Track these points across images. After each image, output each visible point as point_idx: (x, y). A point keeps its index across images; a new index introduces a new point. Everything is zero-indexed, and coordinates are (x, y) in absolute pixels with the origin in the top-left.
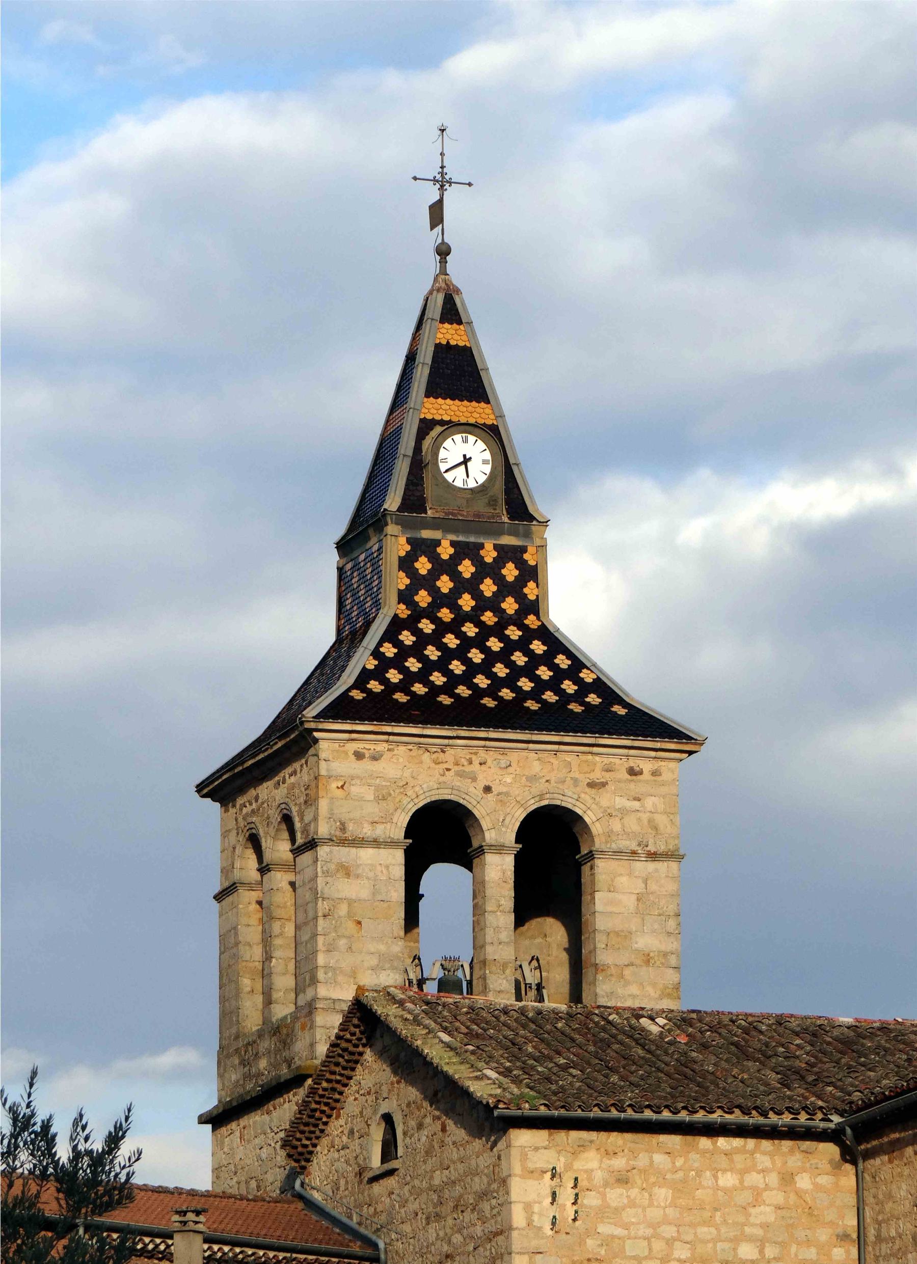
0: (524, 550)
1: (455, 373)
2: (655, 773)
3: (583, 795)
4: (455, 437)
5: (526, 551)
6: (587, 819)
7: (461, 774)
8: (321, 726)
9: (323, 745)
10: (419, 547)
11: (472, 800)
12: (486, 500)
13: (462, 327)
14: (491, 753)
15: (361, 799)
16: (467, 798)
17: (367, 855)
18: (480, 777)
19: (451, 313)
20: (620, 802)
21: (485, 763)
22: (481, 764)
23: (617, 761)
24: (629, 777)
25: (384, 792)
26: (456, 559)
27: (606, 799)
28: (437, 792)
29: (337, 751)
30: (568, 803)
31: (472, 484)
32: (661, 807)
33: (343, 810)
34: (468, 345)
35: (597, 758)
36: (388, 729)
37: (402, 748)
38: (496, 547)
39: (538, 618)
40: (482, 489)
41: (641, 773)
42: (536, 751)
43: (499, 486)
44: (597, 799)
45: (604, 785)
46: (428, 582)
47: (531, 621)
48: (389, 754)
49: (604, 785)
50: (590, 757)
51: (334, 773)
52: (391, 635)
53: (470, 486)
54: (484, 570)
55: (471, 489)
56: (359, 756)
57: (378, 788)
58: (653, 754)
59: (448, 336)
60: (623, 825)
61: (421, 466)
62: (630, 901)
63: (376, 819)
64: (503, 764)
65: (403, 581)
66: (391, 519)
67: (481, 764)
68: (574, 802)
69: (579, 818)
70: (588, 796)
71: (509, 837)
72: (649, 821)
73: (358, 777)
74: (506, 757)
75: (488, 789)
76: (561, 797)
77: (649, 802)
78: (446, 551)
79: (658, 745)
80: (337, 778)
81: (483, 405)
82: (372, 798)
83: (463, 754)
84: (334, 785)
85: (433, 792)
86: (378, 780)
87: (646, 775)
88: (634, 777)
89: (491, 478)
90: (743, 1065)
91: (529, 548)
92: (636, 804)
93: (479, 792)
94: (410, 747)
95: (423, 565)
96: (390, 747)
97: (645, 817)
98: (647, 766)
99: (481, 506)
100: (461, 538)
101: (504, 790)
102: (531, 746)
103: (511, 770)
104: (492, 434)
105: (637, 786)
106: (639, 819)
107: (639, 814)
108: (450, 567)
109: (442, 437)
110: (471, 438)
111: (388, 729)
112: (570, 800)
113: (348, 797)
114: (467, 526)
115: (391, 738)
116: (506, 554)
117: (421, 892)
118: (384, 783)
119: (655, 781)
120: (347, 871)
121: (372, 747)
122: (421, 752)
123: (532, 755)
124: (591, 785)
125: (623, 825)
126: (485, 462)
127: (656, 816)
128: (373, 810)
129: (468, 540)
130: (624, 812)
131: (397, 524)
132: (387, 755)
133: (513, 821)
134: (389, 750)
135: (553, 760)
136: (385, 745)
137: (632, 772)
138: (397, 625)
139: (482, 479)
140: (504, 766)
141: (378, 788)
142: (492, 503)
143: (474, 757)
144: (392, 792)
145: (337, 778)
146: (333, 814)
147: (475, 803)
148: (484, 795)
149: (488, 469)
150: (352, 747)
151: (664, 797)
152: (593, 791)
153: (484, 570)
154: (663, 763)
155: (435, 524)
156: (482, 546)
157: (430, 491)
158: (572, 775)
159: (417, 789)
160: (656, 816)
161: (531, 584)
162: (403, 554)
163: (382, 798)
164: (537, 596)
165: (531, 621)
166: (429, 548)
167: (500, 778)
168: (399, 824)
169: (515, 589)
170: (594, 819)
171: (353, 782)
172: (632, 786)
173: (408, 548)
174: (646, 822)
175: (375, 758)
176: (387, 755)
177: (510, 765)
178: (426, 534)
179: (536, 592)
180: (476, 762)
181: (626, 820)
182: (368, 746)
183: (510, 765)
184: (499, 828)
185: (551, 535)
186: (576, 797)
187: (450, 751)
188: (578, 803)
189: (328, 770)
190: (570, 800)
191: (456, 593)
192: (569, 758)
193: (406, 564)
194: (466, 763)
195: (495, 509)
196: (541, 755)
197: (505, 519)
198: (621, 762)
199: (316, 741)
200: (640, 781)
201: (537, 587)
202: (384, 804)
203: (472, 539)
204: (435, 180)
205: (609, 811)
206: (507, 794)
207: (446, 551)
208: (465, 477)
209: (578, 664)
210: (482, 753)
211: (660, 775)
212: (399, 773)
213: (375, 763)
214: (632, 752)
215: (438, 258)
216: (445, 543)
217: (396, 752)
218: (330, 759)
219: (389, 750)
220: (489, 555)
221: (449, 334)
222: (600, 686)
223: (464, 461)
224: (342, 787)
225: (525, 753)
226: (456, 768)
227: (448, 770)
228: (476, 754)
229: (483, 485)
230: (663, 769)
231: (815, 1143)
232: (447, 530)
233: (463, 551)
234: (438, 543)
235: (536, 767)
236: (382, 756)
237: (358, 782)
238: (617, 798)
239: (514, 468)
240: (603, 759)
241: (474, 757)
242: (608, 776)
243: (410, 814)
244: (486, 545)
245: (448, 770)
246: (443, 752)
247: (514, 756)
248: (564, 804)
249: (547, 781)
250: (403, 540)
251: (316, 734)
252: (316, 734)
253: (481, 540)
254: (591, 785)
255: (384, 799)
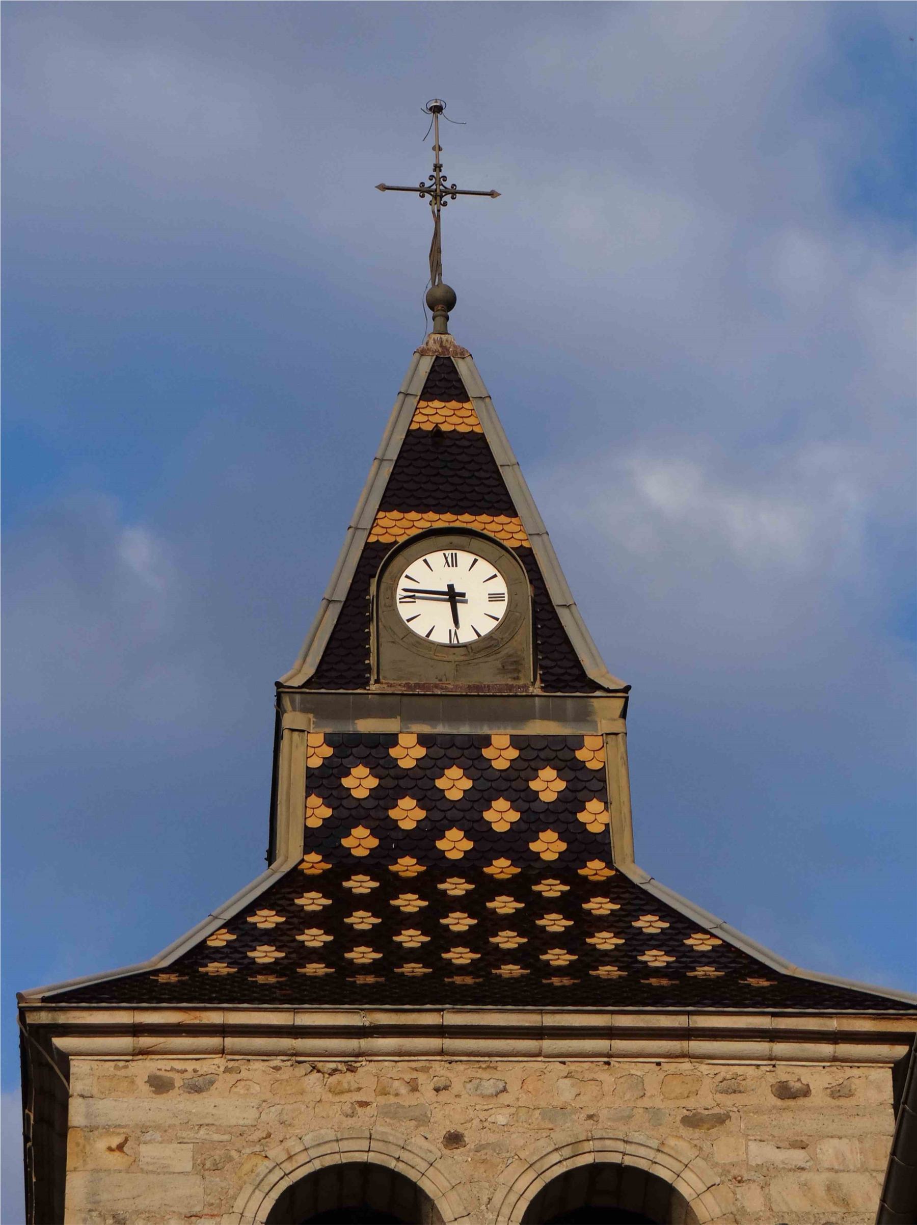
0: (579, 742)
1: (449, 481)
2: (837, 1092)
3: (672, 1142)
4: (429, 557)
5: (581, 746)
6: (683, 1189)
7: (392, 1113)
8: (63, 1018)
9: (78, 1066)
10: (348, 749)
11: (417, 1161)
12: (498, 664)
13: (466, 405)
14: (461, 1067)
15: (165, 1170)
16: (405, 1156)
18: (437, 1115)
19: (444, 382)
20: (762, 1153)
21: (446, 1088)
22: (437, 1090)
23: (751, 1071)
24: (779, 1103)
25: (218, 1154)
26: (431, 767)
27: (726, 1148)
28: (335, 1147)
29: (111, 1078)
30: (639, 1158)
31: (466, 636)
32: (854, 1160)
34: (477, 430)
35: (704, 1068)
36: (215, 1018)
37: (258, 1066)
38: (516, 741)
39: (610, 865)
40: (486, 645)
41: (806, 1092)
42: (562, 1056)
43: (524, 642)
44: (706, 1146)
45: (721, 1120)
46: (374, 814)
47: (594, 869)
48: (231, 1078)
49: (721, 1120)
50: (686, 1066)
51: (102, 1121)
53: (462, 640)
54: (489, 785)
55: (465, 646)
56: (159, 1085)
57: (201, 1147)
58: (826, 1049)
59: (438, 419)
60: (768, 1199)
63: (197, 1209)
64: (489, 1087)
65: (319, 812)
66: (292, 702)
67: (437, 1090)
68: (651, 1154)
69: (669, 1190)
70: (682, 1144)
72: (829, 1189)
73: (157, 1127)
74: (497, 1075)
75: (454, 1140)
76: (621, 1146)
77: (828, 1151)
78: (408, 753)
79: (833, 1025)
80: (108, 1130)
81: (502, 519)
82: (188, 1167)
83: (396, 1072)
84: (101, 1145)
85: (326, 1149)
86: (202, 1131)
87: (818, 1098)
88: (791, 1103)
89: (507, 624)
91: (587, 741)
92: (798, 1156)
93: (436, 1147)
94: (277, 1061)
95: (360, 782)
96: (231, 1064)
97: (819, 1180)
98: (818, 1079)
99: (486, 675)
100: (441, 729)
101: (492, 1138)
102: (548, 1045)
103: (505, 1099)
105: (797, 1120)
106: (805, 1187)
107: (804, 1176)
109: (600, 800)
110: (465, 558)
111: (215, 1018)
112: (642, 1151)
113: (134, 1165)
115: (231, 1042)
116: (534, 753)
118: (216, 1137)
119: (839, 1107)
121: (190, 1066)
122: (301, 1070)
123: (556, 1067)
124: (692, 1121)
125: (768, 1199)
126: (494, 598)
127: (844, 1178)
129: (455, 732)
130: (768, 1173)
131: (304, 710)
132: (223, 1082)
133: (513, 1198)
134: (227, 1070)
135: (605, 1077)
136: (219, 1062)
137: (785, 1092)
139: (487, 627)
140: (492, 1091)
141: (201, 1147)
142: (512, 666)
143: (422, 1078)
144: (234, 1154)
145: (108, 1130)
146: (97, 1202)
147: (423, 1166)
148: (446, 1152)
149: (500, 609)
150: (144, 1068)
151: (861, 1139)
152: (697, 1133)
153: (489, 785)
154: (855, 1072)
155: (388, 705)
156: (486, 741)
157: (384, 656)
158: (646, 1103)
159: (289, 1143)
160: (844, 1178)
161: (594, 806)
162: (315, 762)
163: (209, 1164)
164: (607, 825)
165: (594, 869)
166: (375, 750)
167: (483, 1115)
168: (249, 1215)
169: (563, 815)
170: (701, 1187)
171: (148, 1137)
172: (787, 1119)
173: (328, 751)
174: (821, 1192)
175: (196, 1089)
176: (223, 1082)
177: (504, 1090)
178: (366, 726)
179: (604, 818)
180: (426, 1084)
181: (774, 1190)
182: (179, 1065)
183: (504, 1090)
186: (654, 1144)
187: (366, 1069)
188: (660, 1158)
189: (88, 1115)
190: (642, 1151)
191: (431, 830)
192: (637, 1069)
193: (323, 781)
194: (404, 1090)
195: (518, 678)
196: (573, 1066)
197: (536, 690)
198: (759, 1072)
199: (64, 1059)
200: (803, 1109)
201: (606, 809)
202: (216, 1179)
203: (465, 729)
204: (422, 190)
205: (735, 1172)
206: (497, 1147)
207: (408, 753)
208: (453, 628)
210: (439, 1067)
211: (850, 1095)
212: (251, 1115)
213: (196, 1096)
214: (781, 1048)
215: (430, 313)
216: (407, 740)
217: (244, 1074)
218: (95, 1091)
219: (227, 1070)
220: (501, 754)
221: (442, 415)
224: (120, 1147)
225: (536, 1065)
226: (382, 1100)
227: (364, 1104)
228: (425, 1070)
229: (490, 636)
230: (856, 1084)
232: (410, 717)
234: (392, 740)
235: (566, 1091)
236: (212, 1083)
237: (158, 1136)
238: (753, 1146)
239: (565, 617)
240: (717, 1069)
241: (422, 1078)
242: (728, 1101)
243: (275, 1195)
244: (495, 740)
245: (364, 1104)
246: (352, 1070)
247: (512, 1072)
248: (628, 1161)
249: (590, 1117)
250: (317, 739)
251: (60, 1042)
252: (60, 1042)
253: (485, 730)
254: (692, 1121)
255: (216, 1168)
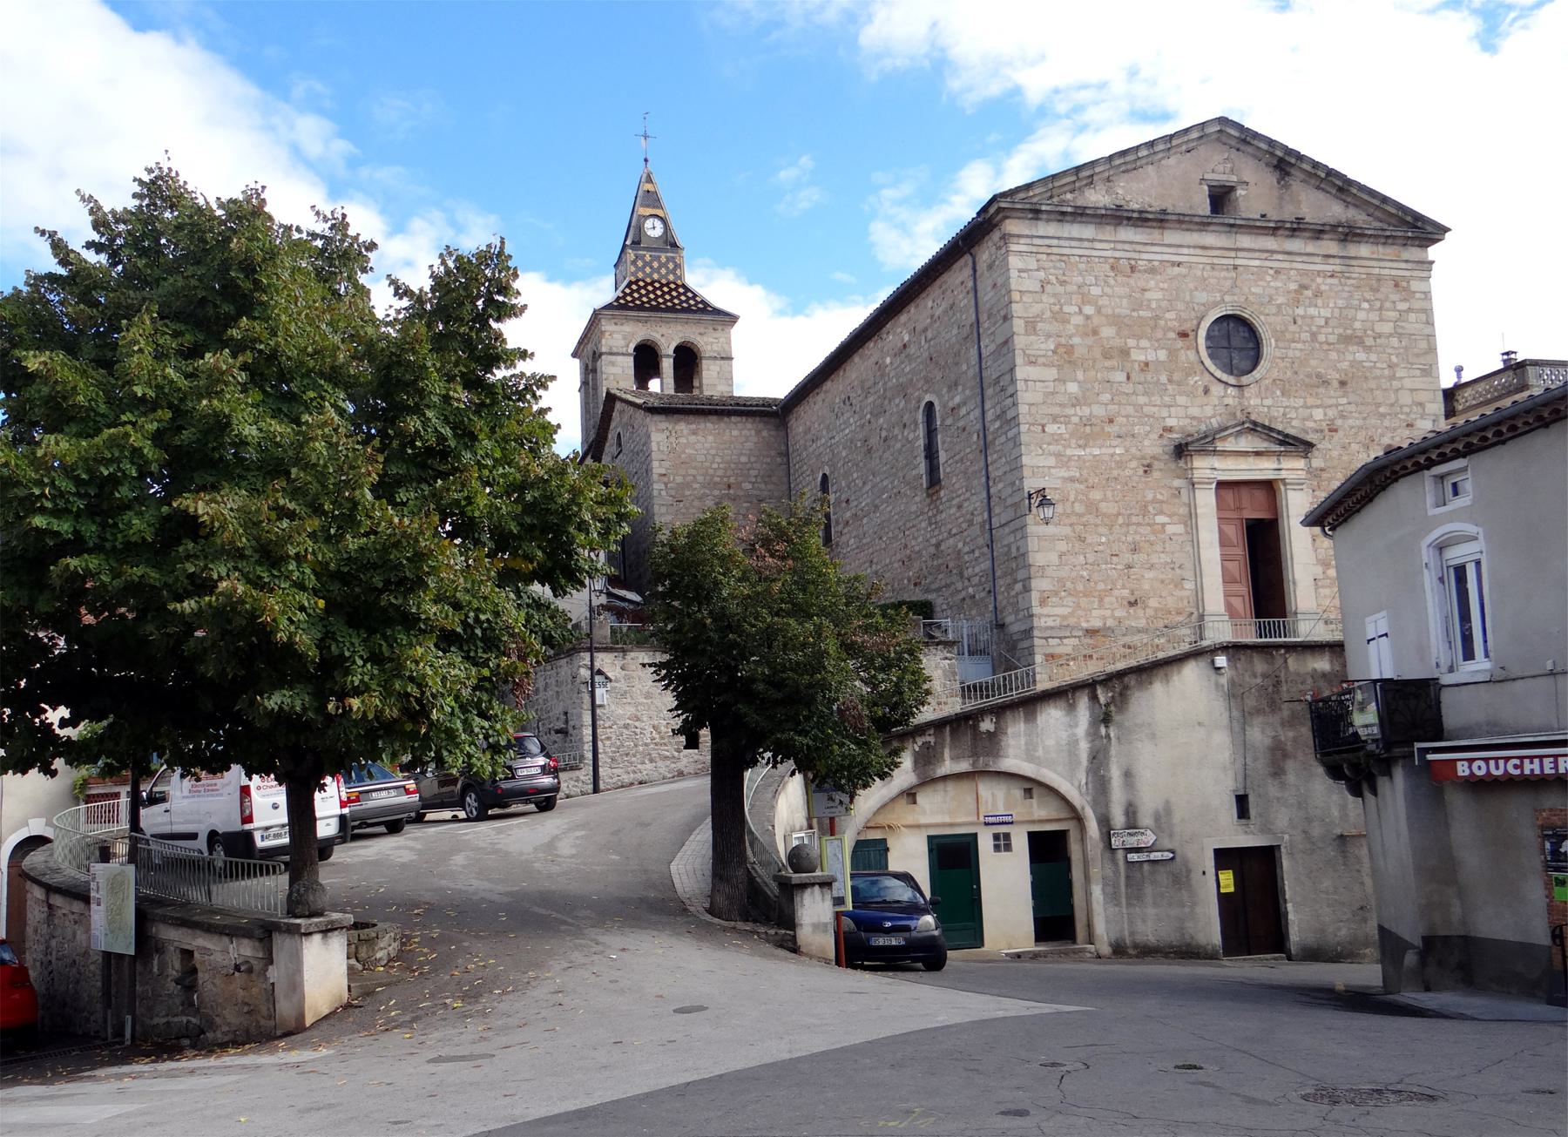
1: (651, 199)
17: (620, 358)
19: (649, 180)
33: (611, 342)
52: (628, 286)
61: (640, 229)
62: (715, 374)
71: (671, 352)
90: (602, 415)
95: (640, 263)
104: (663, 220)
108: (649, 264)
114: (655, 249)
117: (577, 361)
120: (613, 364)
128: (622, 343)
138: (630, 283)
169: (673, 272)
184: (668, 348)
185: (684, 253)
193: (634, 263)
209: (695, 295)
220: (663, 260)
221: (648, 187)
222: (703, 302)
223: (654, 229)
231: (1349, 473)
233: (654, 258)
